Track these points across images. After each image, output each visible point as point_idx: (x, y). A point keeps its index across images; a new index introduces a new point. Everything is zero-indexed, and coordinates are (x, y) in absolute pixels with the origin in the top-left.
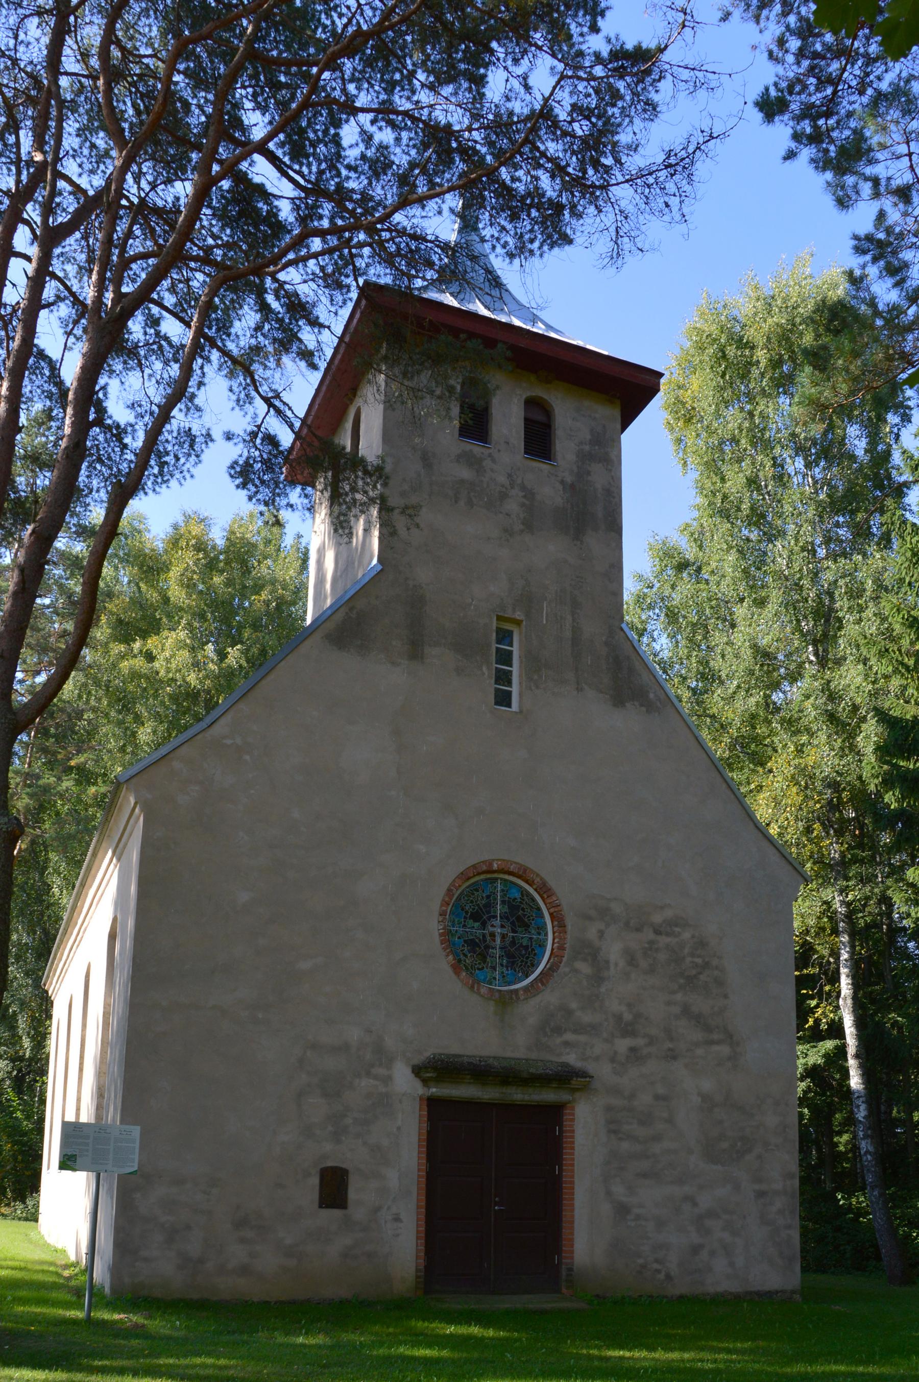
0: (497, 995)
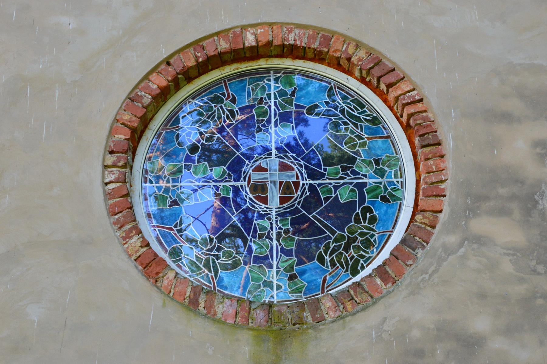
0: (260, 315)
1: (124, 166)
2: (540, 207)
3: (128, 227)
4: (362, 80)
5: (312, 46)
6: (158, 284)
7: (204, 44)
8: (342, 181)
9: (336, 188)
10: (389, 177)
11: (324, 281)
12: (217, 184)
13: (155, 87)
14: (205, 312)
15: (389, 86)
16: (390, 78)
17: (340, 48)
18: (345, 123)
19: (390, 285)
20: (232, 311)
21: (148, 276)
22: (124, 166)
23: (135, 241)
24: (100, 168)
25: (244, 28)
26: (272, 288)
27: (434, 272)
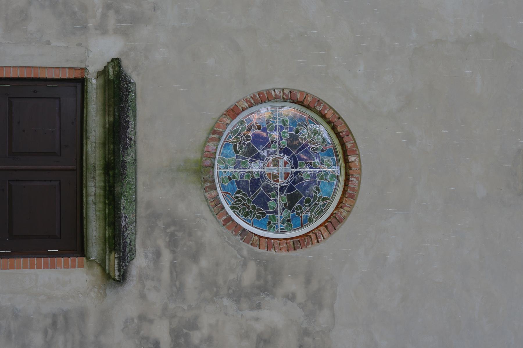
0: (208, 163)
1: (283, 98)
2: (261, 294)
3: (252, 101)
4: (332, 214)
5: (348, 190)
6: (224, 116)
7: (350, 136)
8: (279, 203)
9: (275, 200)
10: (281, 226)
11: (229, 194)
12: (278, 143)
13: (326, 112)
14: (210, 137)
15: (326, 227)
16: (330, 227)
17: (347, 203)
18: (310, 206)
19: (223, 223)
20: (210, 149)
21: (228, 111)
22: (283, 98)
23: (245, 105)
24: (282, 87)
25: (359, 155)
26: (224, 169)
27: (229, 243)
